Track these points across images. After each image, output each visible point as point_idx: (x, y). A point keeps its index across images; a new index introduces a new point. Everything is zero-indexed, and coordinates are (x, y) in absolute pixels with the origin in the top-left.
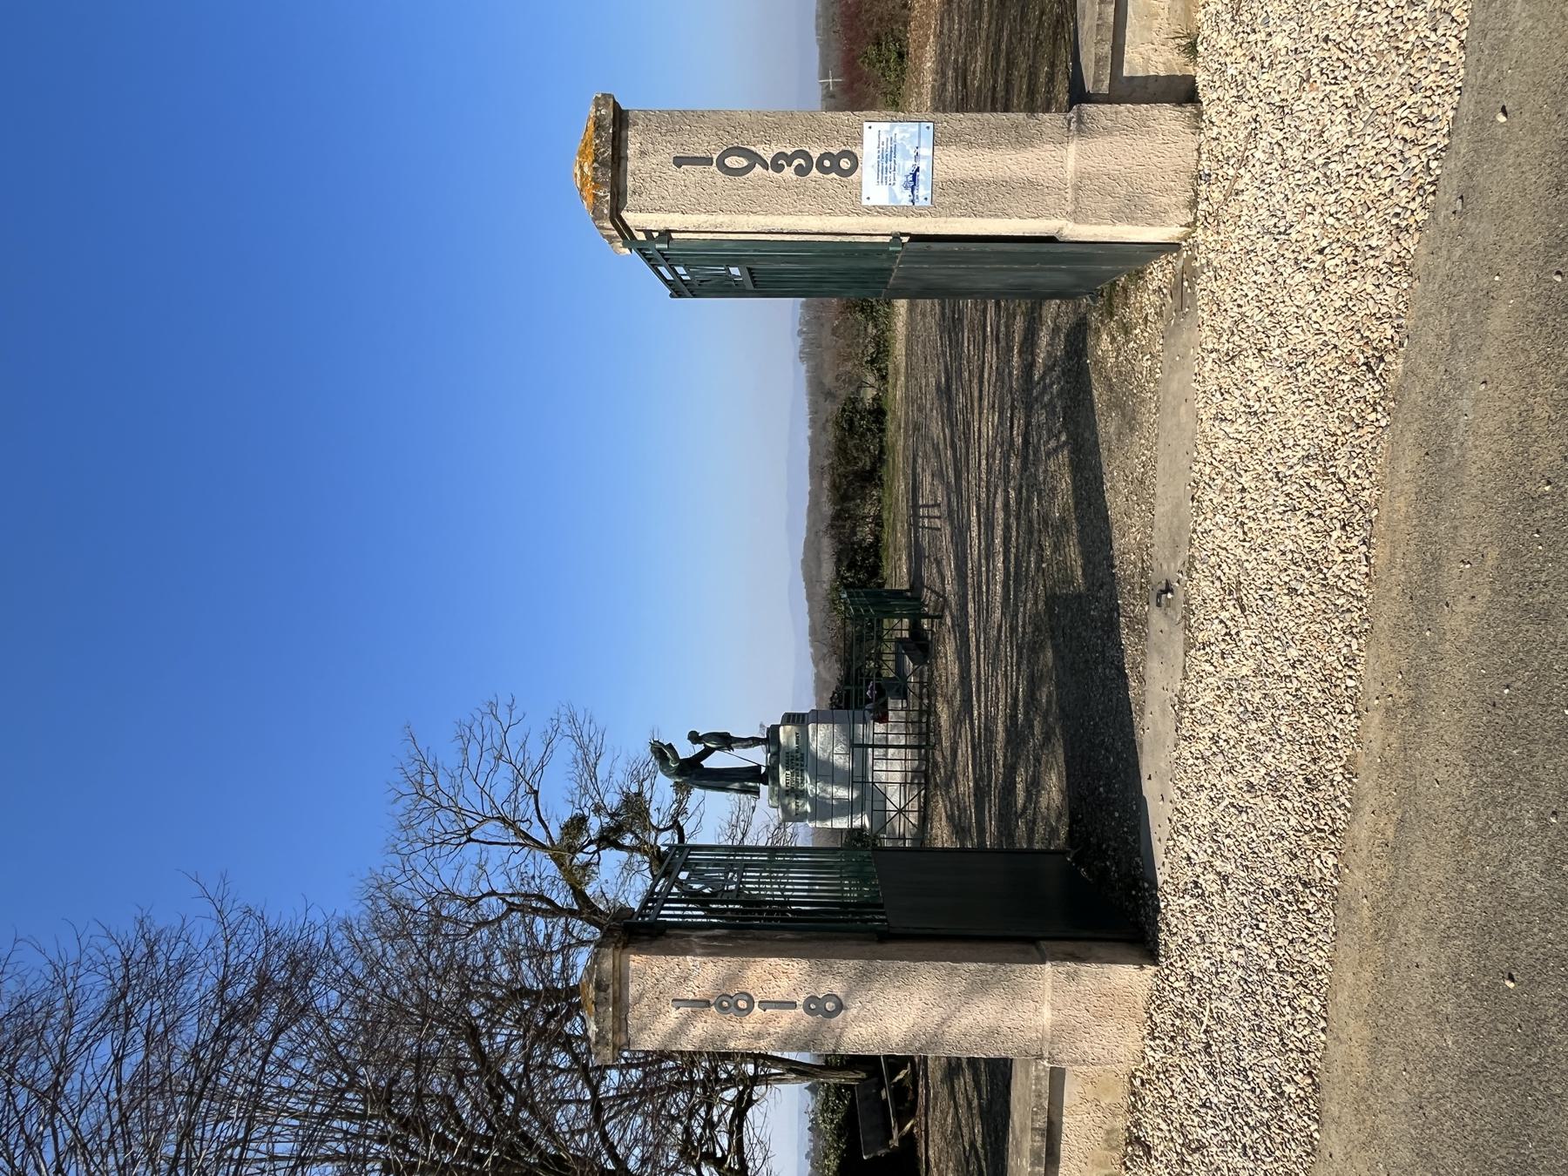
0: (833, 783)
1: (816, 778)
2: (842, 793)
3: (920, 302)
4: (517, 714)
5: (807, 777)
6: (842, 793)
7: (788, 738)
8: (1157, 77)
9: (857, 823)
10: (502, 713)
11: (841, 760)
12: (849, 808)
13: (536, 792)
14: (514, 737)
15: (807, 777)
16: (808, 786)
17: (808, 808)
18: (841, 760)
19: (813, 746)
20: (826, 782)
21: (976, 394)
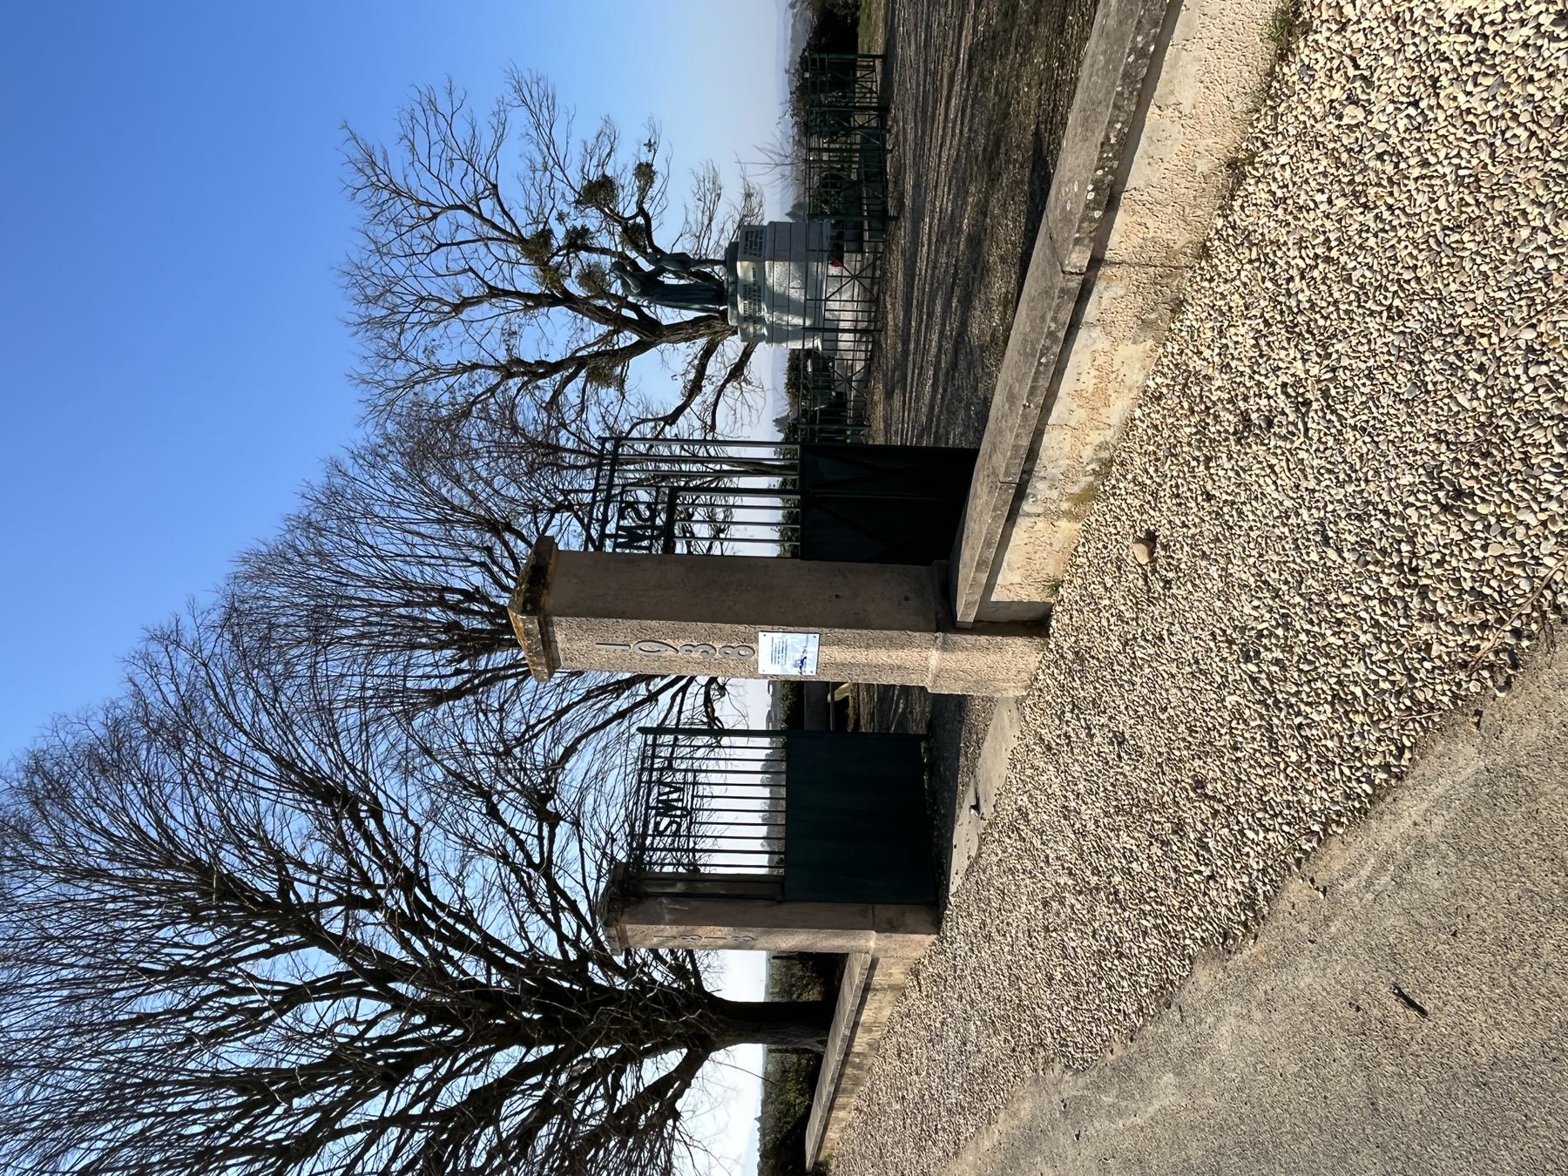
0: (788, 313)
1: (772, 308)
2: (798, 321)
3: (783, 803)
4: (457, 95)
5: (764, 306)
6: (798, 321)
7: (745, 273)
8: (1020, 602)
9: (809, 345)
10: (444, 106)
11: (796, 294)
12: (804, 333)
13: (495, 187)
14: (462, 132)
15: (764, 306)
16: (765, 313)
17: (765, 331)
18: (796, 294)
19: (770, 281)
20: (782, 312)
21: (945, 93)
